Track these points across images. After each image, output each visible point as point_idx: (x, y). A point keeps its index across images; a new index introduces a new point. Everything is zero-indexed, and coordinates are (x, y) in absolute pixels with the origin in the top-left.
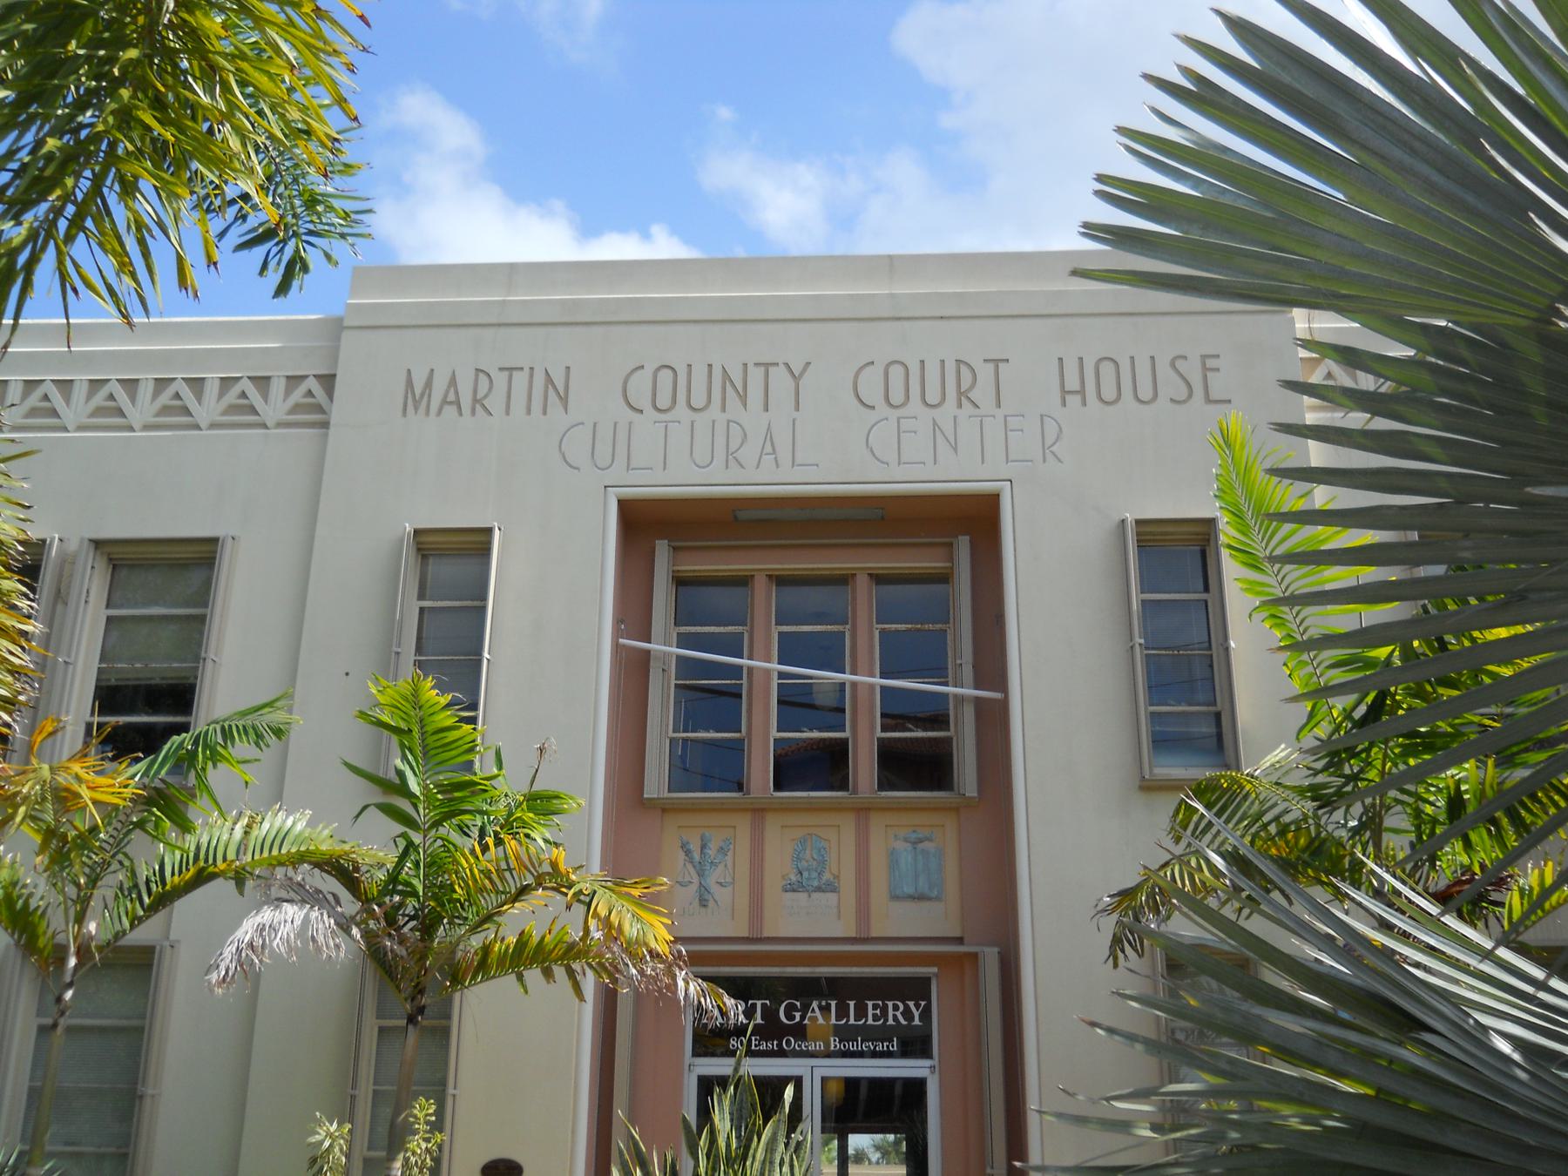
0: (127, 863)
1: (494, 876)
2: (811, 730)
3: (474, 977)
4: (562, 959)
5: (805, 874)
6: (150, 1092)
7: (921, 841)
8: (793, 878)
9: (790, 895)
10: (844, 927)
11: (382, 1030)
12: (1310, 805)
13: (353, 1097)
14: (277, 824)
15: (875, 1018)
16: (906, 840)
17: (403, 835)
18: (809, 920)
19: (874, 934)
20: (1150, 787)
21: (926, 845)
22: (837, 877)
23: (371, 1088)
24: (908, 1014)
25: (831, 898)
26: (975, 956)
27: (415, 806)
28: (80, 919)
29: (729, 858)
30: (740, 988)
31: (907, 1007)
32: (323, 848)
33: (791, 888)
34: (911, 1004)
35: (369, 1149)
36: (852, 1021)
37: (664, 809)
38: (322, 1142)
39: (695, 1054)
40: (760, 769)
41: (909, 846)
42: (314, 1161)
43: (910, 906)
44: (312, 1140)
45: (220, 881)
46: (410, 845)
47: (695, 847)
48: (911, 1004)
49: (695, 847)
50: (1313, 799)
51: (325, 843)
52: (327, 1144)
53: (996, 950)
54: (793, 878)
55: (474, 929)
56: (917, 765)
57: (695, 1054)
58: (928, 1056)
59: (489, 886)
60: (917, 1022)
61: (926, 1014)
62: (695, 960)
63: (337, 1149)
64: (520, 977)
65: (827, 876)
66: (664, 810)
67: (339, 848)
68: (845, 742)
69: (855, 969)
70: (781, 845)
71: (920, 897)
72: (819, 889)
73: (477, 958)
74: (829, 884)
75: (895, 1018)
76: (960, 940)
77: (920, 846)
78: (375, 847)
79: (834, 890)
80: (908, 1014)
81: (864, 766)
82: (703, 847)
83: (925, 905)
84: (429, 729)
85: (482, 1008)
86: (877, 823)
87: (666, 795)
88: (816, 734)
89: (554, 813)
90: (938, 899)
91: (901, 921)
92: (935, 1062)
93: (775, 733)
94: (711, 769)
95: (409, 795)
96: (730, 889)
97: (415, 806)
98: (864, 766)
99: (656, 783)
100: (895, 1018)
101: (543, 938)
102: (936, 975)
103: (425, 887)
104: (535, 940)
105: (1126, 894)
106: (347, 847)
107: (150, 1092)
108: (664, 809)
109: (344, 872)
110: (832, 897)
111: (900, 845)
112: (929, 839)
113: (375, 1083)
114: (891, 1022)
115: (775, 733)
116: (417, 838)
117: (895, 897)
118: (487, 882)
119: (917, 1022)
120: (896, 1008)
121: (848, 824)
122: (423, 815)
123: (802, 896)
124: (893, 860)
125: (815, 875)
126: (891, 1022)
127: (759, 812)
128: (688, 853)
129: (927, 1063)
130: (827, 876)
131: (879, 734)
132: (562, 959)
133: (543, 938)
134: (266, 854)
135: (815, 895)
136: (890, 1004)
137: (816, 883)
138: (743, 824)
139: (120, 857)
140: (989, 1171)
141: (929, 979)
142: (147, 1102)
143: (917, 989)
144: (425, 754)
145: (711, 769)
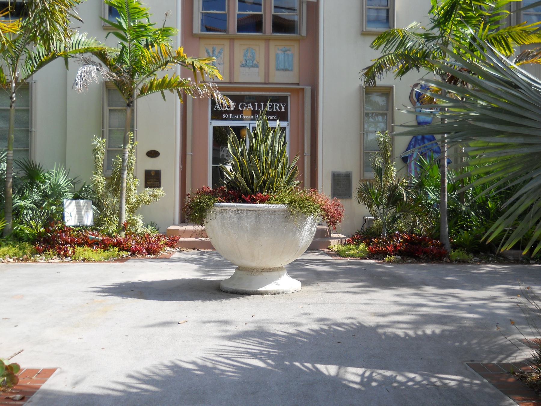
0: (26, 51)
1: (156, 58)
2: (250, 11)
3: (148, 92)
4: (176, 86)
5: (248, 61)
6: (34, 130)
7: (286, 51)
8: (244, 63)
9: (243, 68)
10: (261, 79)
11: (110, 110)
12: (423, 40)
13: (103, 131)
14: (76, 38)
15: (270, 108)
16: (282, 51)
17: (121, 43)
18: (249, 76)
19: (270, 82)
20: (364, 34)
21: (288, 52)
22: (258, 63)
23: (108, 128)
24: (280, 108)
25: (256, 69)
26: (303, 89)
27: (126, 33)
28: (14, 71)
29: (222, 55)
30: (233, 98)
31: (280, 105)
32: (93, 47)
33: (243, 66)
34: (281, 104)
35: (109, 147)
36: (256, 109)
37: (200, 37)
38: (97, 144)
39: (212, 119)
40: (233, 24)
41: (282, 53)
42: (94, 150)
43: (283, 73)
44: (93, 144)
45: (60, 58)
46: (124, 47)
47: (210, 51)
48: (281, 104)
49: (210, 51)
50: (425, 38)
51: (93, 44)
52: (99, 145)
53: (310, 87)
54: (244, 63)
55: (148, 76)
56: (282, 26)
57: (212, 119)
58: (286, 120)
59: (155, 62)
60: (283, 110)
61: (286, 108)
62: (220, 89)
63: (102, 147)
64: (162, 92)
65: (255, 62)
66: (200, 38)
67: (100, 46)
68: (261, 15)
69: (264, 93)
70: (240, 50)
71: (286, 70)
72: (252, 66)
73: (149, 86)
74: (255, 65)
75: (276, 109)
76: (298, 84)
77: (286, 52)
78: (113, 47)
79: (257, 67)
80: (280, 108)
81: (268, 24)
82: (213, 51)
83: (287, 72)
84: (130, 7)
85: (142, 104)
86: (272, 44)
87: (200, 32)
88: (251, 13)
89: (169, 36)
90: (291, 70)
91: (279, 77)
92: (289, 122)
93: (237, 12)
94: (213, 25)
95: (123, 29)
96: (222, 66)
97: (126, 33)
98: (268, 24)
99: (197, 28)
100: (276, 109)
101: (171, 80)
102: (290, 95)
103: (130, 62)
104: (168, 80)
105: (370, 68)
106: (101, 46)
107: (34, 130)
108: (200, 37)
109: (102, 55)
110: (257, 69)
111: (280, 52)
112: (289, 50)
113: (109, 127)
114: (275, 110)
115: (237, 12)
116: (126, 45)
117: (278, 70)
118: (153, 60)
119: (283, 110)
120: (276, 105)
121: (262, 44)
122: (129, 36)
123: (247, 69)
124: (277, 56)
125: (251, 61)
126: (275, 110)
127: (232, 39)
128: (208, 53)
129: (286, 123)
130: (255, 62)
131: (273, 13)
132: (176, 86)
133: (171, 80)
134: (74, 49)
135: (251, 69)
136: (275, 104)
137: (251, 64)
138: (227, 43)
139: (24, 49)
140: (305, 155)
141: (287, 97)
142: (33, 133)
143: (283, 100)
144: (129, 15)
145: (213, 25)
